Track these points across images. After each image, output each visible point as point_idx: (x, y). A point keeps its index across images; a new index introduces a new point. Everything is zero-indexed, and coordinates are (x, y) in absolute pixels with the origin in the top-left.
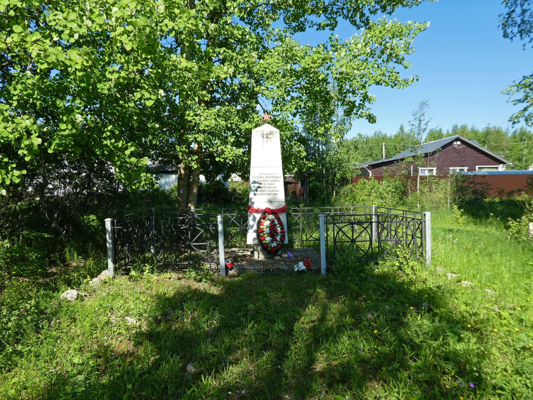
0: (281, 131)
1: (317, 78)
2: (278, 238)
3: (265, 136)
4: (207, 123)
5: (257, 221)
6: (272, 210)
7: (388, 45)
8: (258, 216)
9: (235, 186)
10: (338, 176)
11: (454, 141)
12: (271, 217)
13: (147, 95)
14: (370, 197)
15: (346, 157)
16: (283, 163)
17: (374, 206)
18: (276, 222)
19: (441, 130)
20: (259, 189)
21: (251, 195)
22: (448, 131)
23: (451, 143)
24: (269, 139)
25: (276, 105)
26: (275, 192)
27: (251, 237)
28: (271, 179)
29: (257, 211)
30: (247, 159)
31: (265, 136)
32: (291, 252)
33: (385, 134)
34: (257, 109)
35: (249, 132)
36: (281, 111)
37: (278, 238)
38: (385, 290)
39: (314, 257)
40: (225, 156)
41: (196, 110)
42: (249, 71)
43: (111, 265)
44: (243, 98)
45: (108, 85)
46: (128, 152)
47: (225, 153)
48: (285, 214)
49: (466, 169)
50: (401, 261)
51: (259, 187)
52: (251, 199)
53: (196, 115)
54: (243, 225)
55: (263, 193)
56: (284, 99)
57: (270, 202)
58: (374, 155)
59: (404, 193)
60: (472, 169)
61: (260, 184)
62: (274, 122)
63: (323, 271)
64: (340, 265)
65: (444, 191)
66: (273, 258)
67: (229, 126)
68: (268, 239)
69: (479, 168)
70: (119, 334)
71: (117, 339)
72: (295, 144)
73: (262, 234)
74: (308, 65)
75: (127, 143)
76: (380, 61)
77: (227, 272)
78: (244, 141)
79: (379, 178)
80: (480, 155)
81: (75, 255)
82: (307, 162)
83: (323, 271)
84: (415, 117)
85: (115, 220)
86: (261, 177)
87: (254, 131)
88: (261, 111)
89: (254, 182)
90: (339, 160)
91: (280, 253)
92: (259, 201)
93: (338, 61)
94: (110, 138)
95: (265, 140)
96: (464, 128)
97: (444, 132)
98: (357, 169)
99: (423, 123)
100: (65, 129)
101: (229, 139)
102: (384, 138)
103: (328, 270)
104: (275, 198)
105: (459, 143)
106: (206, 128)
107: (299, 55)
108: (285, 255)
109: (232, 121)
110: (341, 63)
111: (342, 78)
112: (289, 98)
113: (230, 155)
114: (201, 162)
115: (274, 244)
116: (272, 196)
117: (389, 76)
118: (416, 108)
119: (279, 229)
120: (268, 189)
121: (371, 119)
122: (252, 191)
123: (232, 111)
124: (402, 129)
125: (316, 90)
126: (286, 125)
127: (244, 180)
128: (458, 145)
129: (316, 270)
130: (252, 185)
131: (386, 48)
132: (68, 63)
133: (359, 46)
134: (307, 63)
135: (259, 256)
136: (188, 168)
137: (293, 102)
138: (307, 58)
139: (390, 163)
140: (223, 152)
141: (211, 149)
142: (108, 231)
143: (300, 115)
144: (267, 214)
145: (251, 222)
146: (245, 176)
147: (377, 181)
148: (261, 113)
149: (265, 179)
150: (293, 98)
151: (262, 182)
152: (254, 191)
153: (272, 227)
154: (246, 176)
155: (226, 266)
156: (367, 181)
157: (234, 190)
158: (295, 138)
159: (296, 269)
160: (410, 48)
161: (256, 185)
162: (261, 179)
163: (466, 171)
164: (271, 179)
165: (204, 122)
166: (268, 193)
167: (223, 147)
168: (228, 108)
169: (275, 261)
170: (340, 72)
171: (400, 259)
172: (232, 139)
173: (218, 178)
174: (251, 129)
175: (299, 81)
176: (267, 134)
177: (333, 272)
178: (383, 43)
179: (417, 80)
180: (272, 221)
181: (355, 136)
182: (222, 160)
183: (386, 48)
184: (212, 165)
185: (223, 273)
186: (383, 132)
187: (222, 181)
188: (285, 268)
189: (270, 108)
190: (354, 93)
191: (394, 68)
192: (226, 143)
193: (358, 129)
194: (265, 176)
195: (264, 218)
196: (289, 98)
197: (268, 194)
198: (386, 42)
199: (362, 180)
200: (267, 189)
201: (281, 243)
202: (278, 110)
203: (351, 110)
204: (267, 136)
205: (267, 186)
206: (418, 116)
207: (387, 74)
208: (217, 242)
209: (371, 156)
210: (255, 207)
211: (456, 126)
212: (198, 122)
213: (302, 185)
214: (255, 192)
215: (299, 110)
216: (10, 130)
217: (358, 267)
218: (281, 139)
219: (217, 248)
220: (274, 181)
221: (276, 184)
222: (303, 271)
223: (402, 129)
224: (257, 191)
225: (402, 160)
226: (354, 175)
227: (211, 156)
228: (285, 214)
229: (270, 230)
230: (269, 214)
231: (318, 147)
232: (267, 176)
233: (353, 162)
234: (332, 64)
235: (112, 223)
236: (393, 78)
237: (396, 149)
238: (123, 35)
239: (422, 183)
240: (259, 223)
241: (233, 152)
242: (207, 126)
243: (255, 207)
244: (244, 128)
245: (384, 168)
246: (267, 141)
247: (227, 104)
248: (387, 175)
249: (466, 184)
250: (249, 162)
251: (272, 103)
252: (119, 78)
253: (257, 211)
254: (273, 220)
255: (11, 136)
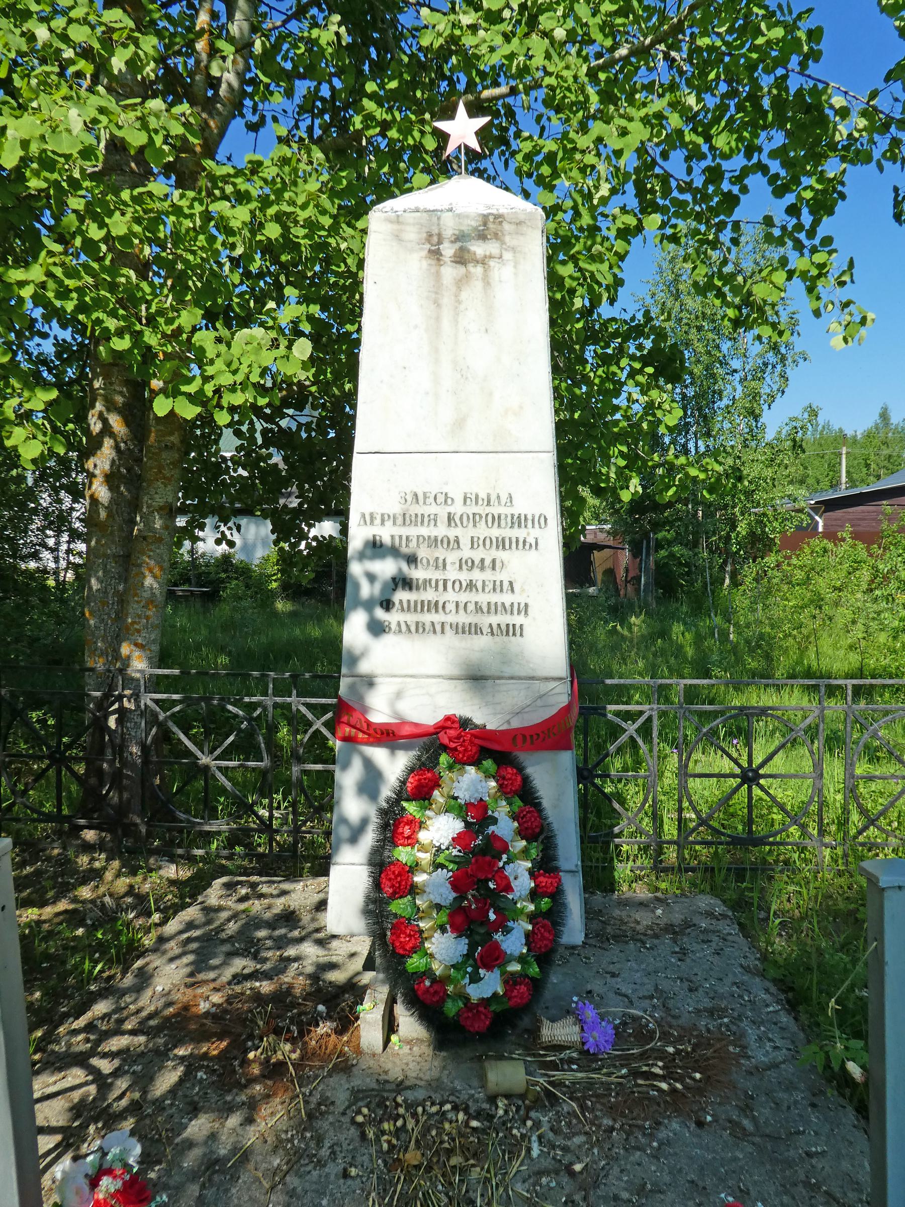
3: (448, 250)
5: (386, 792)
6: (483, 733)
8: (393, 765)
10: (742, 528)
12: (471, 782)
18: (505, 826)
20: (401, 596)
21: (354, 630)
24: (478, 270)
28: (482, 531)
29: (387, 736)
31: (448, 250)
33: (841, 430)
37: (513, 942)
48: (566, 760)
51: (402, 582)
52: (354, 660)
55: (427, 618)
57: (476, 678)
68: (442, 949)
73: (400, 906)
86: (419, 520)
89: (375, 548)
92: (405, 673)
95: (450, 272)
98: (800, 511)
104: (505, 657)
115: (490, 984)
116: (482, 642)
119: (520, 875)
120: (463, 597)
122: (358, 603)
124: (884, 415)
144: (444, 759)
145: (352, 806)
147: (861, 546)
149: (441, 530)
151: (423, 553)
152: (368, 606)
153: (477, 862)
156: (830, 546)
161: (386, 568)
162: (413, 531)
164: (482, 531)
166: (463, 618)
176: (460, 237)
180: (477, 816)
181: (797, 412)
194: (442, 512)
195: (422, 787)
197: (460, 630)
200: (451, 596)
204: (460, 250)
205: (452, 574)
210: (379, 710)
213: (636, 552)
214: (380, 613)
220: (501, 544)
221: (515, 564)
223: (884, 415)
224: (387, 605)
228: (566, 760)
229: (456, 884)
230: (461, 761)
232: (458, 509)
237: (868, 466)
240: (394, 826)
243: (379, 710)
246: (461, 283)
248: (895, 527)
253: (387, 736)
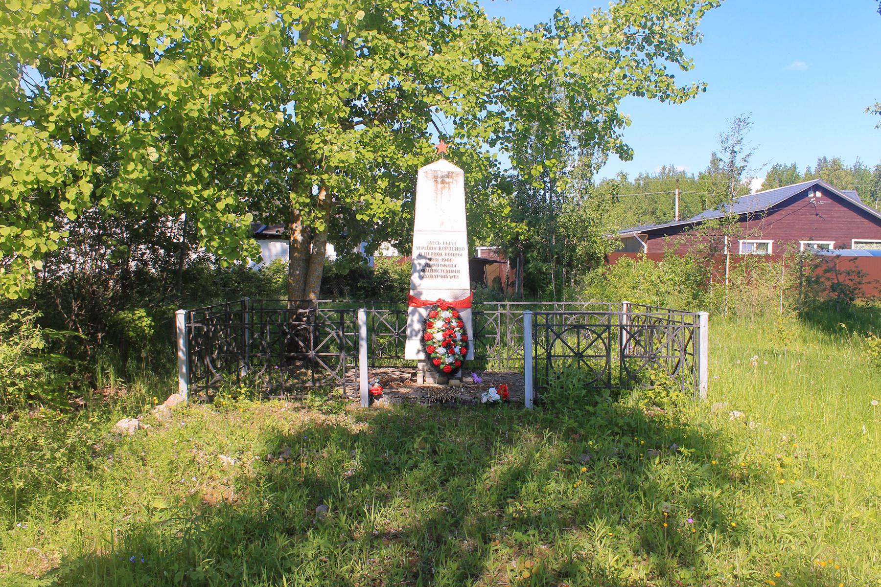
0: (466, 171)
1: (531, 81)
2: (457, 349)
3: (439, 180)
4: (342, 156)
7: (656, 28)
9: (387, 265)
11: (809, 190)
12: (447, 314)
13: (260, 121)
14: (631, 289)
15: (594, 215)
16: (468, 227)
17: (625, 302)
19: (794, 167)
21: (415, 278)
22: (809, 169)
23: (804, 194)
25: (461, 125)
26: (453, 274)
27: (413, 350)
28: (448, 251)
30: (409, 216)
31: (439, 180)
32: (479, 375)
34: (429, 130)
35: (411, 177)
36: (468, 137)
37: (457, 349)
38: (621, 428)
39: (517, 384)
40: (372, 213)
41: (325, 133)
42: (415, 71)
43: (183, 386)
44: (404, 112)
45: (199, 104)
46: (221, 206)
47: (372, 207)
49: (831, 244)
50: (657, 390)
53: (325, 142)
54: (399, 329)
56: (475, 117)
58: (658, 213)
59: (703, 285)
60: (846, 246)
61: (430, 259)
62: (456, 156)
63: (528, 404)
64: (555, 393)
65: (775, 286)
66: (447, 383)
67: (380, 160)
69: (856, 243)
70: (211, 478)
71: (208, 485)
72: (493, 193)
73: (429, 343)
74: (516, 61)
75: (220, 190)
76: (641, 55)
77: (371, 402)
78: (404, 186)
79: (656, 257)
80: (859, 219)
81: (112, 377)
82: (513, 225)
83: (528, 404)
84: (725, 145)
85: (193, 313)
86: (432, 248)
87: (421, 172)
88: (436, 134)
89: (420, 256)
90: (582, 221)
91: (459, 374)
93: (568, 55)
94: (193, 183)
95: (440, 186)
96: (836, 164)
97: (802, 171)
98: (616, 240)
99: (739, 158)
100: (135, 171)
101: (379, 182)
102: (679, 180)
103: (536, 402)
105: (819, 194)
106: (341, 165)
107: (502, 43)
108: (470, 379)
109: (384, 153)
110: (572, 58)
111: (574, 84)
112: (484, 113)
113: (379, 211)
114: (332, 225)
117: (656, 82)
118: (726, 129)
120: (443, 268)
121: (625, 153)
122: (415, 271)
123: (385, 134)
125: (529, 103)
126: (477, 161)
127: (403, 253)
128: (817, 199)
129: (516, 402)
130: (416, 262)
131: (653, 33)
132: (156, 81)
133: (606, 29)
134: (515, 58)
135: (426, 381)
136: (310, 234)
137: (491, 123)
138: (514, 50)
139: (691, 232)
140: (368, 205)
141: (348, 200)
142: (181, 330)
143: (501, 144)
146: (405, 247)
147: (651, 262)
148: (435, 139)
149: (437, 251)
150: (490, 115)
152: (419, 272)
154: (407, 246)
155: (370, 392)
156: (633, 262)
157: (385, 272)
158: (493, 182)
159: (484, 400)
160: (694, 33)
161: (423, 262)
162: (430, 251)
163: (831, 247)
164: (448, 251)
165: (337, 154)
166: (443, 274)
167: (368, 197)
168: (379, 129)
169: (452, 387)
170: (571, 74)
171: (655, 387)
172: (383, 184)
173: (355, 250)
174: (416, 166)
175: (502, 86)
176: (443, 177)
177: (543, 404)
178: (649, 24)
179: (704, 90)
180: (448, 321)
182: (366, 219)
183: (653, 33)
184: (347, 226)
185: (364, 404)
186: (679, 169)
187: (364, 255)
188: (467, 397)
189: (450, 129)
190: (593, 109)
191: (665, 68)
192: (375, 190)
193: (610, 169)
194: (438, 246)
196: (484, 113)
198: (653, 24)
199: (623, 260)
200: (440, 268)
201: (462, 359)
202: (463, 136)
203: (593, 137)
204: (443, 180)
205: (440, 262)
206: (730, 143)
207: (653, 78)
208: (356, 358)
209: (653, 213)
211: (825, 159)
212: (327, 154)
213: (513, 266)
214: (422, 273)
215: (500, 135)
216: (50, 170)
217: (584, 396)
218: (466, 185)
219: (357, 366)
220: (453, 255)
221: (456, 260)
222: (495, 403)
225: (699, 224)
226: (610, 251)
227: (346, 210)
230: (443, 310)
231: (544, 195)
232: (441, 246)
233: (610, 226)
234: (557, 60)
235: (188, 318)
236: (662, 85)
238: (229, 35)
239: (735, 267)
241: (384, 206)
242: (343, 162)
244: (406, 165)
245: (667, 238)
246: (442, 189)
247: (376, 122)
249: (819, 271)
250: (411, 222)
251: (455, 122)
252: (218, 95)
253: (424, 304)
254: (449, 319)
255: (52, 180)
